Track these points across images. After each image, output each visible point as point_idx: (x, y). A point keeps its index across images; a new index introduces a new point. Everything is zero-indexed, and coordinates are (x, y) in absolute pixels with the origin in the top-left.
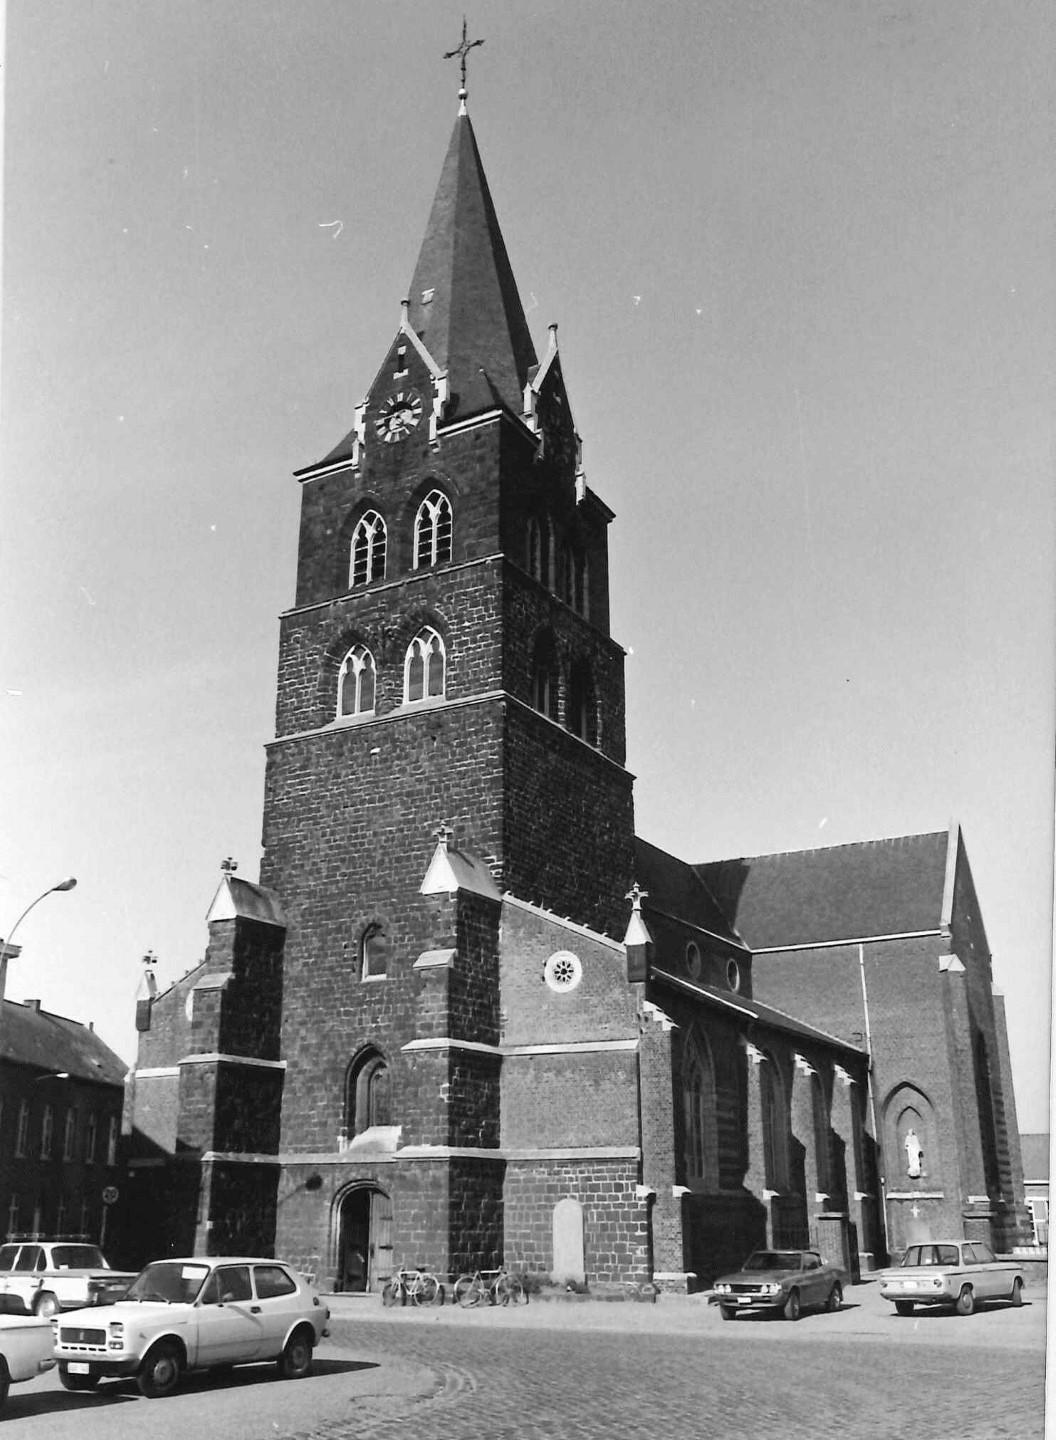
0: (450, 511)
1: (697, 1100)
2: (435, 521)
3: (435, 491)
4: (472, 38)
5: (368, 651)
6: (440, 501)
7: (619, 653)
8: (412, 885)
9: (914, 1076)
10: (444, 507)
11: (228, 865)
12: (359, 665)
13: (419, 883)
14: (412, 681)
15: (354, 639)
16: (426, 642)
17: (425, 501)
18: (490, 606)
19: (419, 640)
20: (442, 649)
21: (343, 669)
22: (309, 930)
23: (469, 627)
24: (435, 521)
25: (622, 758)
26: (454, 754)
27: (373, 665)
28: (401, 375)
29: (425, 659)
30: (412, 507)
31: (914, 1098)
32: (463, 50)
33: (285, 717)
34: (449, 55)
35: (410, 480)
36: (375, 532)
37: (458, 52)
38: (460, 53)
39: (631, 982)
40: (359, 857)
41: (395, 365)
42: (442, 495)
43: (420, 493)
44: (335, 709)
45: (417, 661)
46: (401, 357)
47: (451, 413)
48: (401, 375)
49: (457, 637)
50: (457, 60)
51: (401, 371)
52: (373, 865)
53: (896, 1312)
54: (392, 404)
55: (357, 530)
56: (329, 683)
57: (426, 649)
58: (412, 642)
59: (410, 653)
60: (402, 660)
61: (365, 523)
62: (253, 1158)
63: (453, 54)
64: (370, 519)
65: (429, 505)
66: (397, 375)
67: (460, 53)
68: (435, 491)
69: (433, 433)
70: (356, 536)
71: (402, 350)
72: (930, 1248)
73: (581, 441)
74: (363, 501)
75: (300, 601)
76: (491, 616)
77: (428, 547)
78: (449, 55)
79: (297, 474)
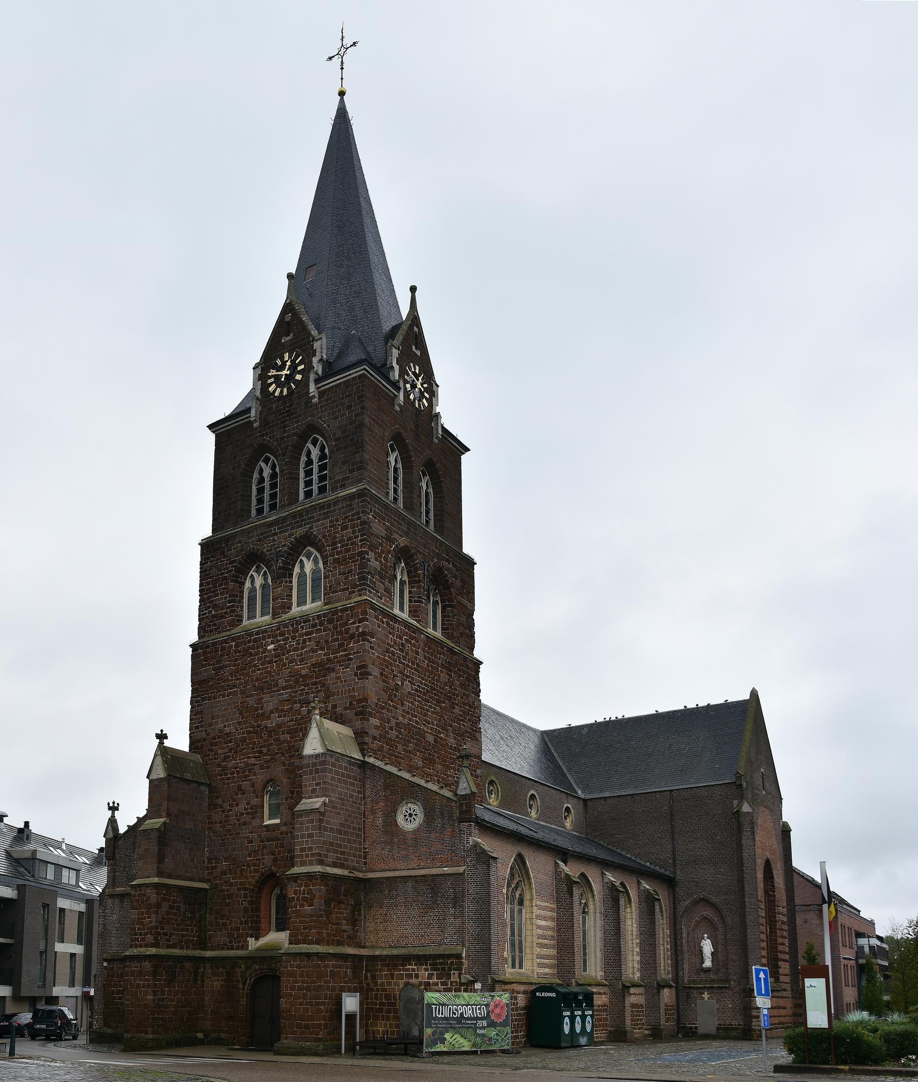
0: (327, 451)
1: (520, 911)
4: (348, 42)
7: (469, 563)
9: (709, 894)
10: (322, 449)
11: (162, 737)
17: (308, 444)
20: (321, 565)
21: (248, 584)
25: (472, 647)
27: (270, 581)
28: (288, 338)
29: (258, 587)
30: (299, 449)
31: (709, 913)
32: (342, 53)
34: (354, 44)
35: (295, 427)
36: (271, 472)
37: (338, 54)
38: (341, 55)
39: (460, 822)
42: (321, 439)
43: (303, 438)
46: (288, 323)
47: (330, 369)
48: (288, 338)
50: (337, 61)
55: (305, 450)
59: (297, 570)
60: (291, 576)
63: (333, 57)
64: (266, 461)
65: (263, 465)
67: (341, 55)
68: (267, 454)
69: (312, 388)
70: (304, 458)
72: (563, 1045)
73: (438, 386)
75: (214, 531)
78: (330, 58)
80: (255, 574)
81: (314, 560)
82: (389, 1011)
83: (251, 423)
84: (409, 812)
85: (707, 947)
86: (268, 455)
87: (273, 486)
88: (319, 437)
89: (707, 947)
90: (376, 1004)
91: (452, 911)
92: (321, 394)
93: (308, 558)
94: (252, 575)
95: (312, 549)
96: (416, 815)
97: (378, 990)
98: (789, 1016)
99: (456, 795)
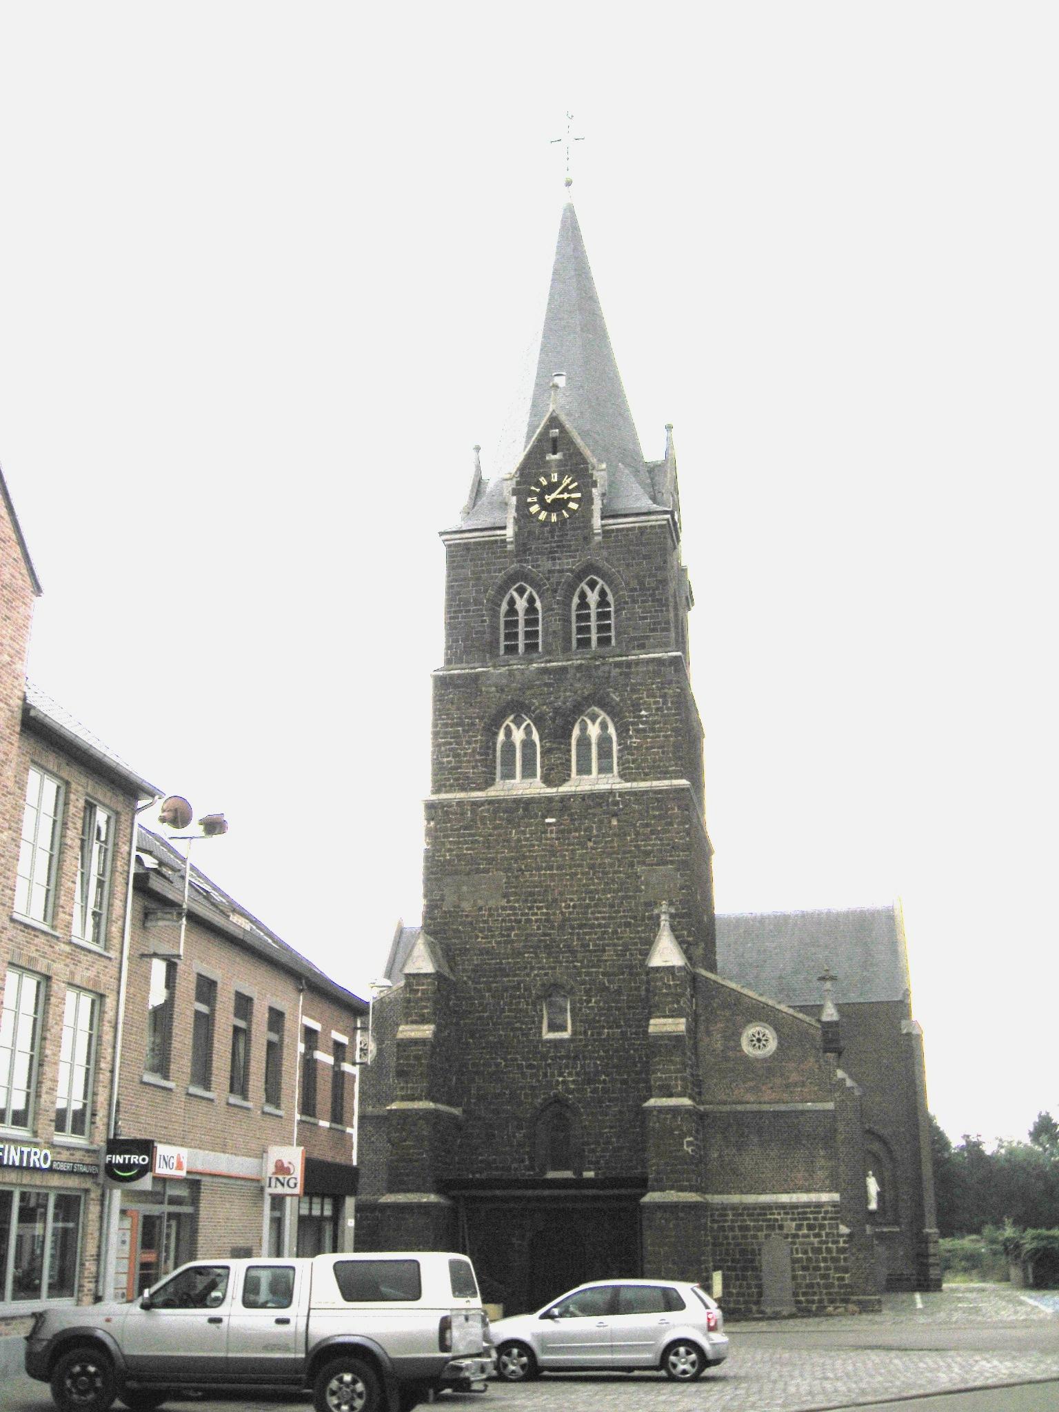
0: (538, 605)
2: (593, 605)
3: (522, 583)
5: (528, 721)
6: (598, 587)
8: (598, 951)
12: (518, 736)
13: (646, 954)
14: (600, 757)
15: (518, 709)
16: (519, 728)
18: (669, 700)
19: (586, 719)
22: (482, 986)
23: (646, 716)
24: (593, 605)
26: (637, 834)
30: (571, 588)
33: (445, 776)
40: (537, 921)
41: (549, 445)
44: (495, 774)
45: (584, 742)
49: (633, 724)
51: (554, 453)
52: (552, 928)
53: (310, 1349)
54: (545, 483)
55: (507, 598)
56: (489, 747)
57: (594, 731)
58: (579, 721)
59: (576, 732)
61: (515, 595)
62: (791, 1198)
66: (551, 457)
68: (522, 583)
71: (555, 432)
74: (516, 573)
76: (668, 709)
77: (528, 635)
79: (441, 534)
80: (513, 726)
81: (525, 729)
82: (745, 1269)
83: (504, 541)
84: (757, 1036)
85: (873, 1186)
86: (595, 578)
87: (531, 622)
88: (599, 580)
89: (873, 1186)
90: (728, 1261)
91: (822, 1153)
92: (606, 533)
93: (593, 721)
94: (508, 726)
95: (596, 709)
96: (766, 1040)
97: (729, 1244)
98: (311, 1203)
99: (819, 1021)
